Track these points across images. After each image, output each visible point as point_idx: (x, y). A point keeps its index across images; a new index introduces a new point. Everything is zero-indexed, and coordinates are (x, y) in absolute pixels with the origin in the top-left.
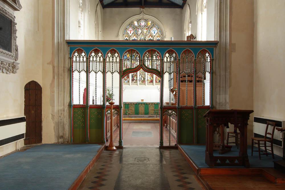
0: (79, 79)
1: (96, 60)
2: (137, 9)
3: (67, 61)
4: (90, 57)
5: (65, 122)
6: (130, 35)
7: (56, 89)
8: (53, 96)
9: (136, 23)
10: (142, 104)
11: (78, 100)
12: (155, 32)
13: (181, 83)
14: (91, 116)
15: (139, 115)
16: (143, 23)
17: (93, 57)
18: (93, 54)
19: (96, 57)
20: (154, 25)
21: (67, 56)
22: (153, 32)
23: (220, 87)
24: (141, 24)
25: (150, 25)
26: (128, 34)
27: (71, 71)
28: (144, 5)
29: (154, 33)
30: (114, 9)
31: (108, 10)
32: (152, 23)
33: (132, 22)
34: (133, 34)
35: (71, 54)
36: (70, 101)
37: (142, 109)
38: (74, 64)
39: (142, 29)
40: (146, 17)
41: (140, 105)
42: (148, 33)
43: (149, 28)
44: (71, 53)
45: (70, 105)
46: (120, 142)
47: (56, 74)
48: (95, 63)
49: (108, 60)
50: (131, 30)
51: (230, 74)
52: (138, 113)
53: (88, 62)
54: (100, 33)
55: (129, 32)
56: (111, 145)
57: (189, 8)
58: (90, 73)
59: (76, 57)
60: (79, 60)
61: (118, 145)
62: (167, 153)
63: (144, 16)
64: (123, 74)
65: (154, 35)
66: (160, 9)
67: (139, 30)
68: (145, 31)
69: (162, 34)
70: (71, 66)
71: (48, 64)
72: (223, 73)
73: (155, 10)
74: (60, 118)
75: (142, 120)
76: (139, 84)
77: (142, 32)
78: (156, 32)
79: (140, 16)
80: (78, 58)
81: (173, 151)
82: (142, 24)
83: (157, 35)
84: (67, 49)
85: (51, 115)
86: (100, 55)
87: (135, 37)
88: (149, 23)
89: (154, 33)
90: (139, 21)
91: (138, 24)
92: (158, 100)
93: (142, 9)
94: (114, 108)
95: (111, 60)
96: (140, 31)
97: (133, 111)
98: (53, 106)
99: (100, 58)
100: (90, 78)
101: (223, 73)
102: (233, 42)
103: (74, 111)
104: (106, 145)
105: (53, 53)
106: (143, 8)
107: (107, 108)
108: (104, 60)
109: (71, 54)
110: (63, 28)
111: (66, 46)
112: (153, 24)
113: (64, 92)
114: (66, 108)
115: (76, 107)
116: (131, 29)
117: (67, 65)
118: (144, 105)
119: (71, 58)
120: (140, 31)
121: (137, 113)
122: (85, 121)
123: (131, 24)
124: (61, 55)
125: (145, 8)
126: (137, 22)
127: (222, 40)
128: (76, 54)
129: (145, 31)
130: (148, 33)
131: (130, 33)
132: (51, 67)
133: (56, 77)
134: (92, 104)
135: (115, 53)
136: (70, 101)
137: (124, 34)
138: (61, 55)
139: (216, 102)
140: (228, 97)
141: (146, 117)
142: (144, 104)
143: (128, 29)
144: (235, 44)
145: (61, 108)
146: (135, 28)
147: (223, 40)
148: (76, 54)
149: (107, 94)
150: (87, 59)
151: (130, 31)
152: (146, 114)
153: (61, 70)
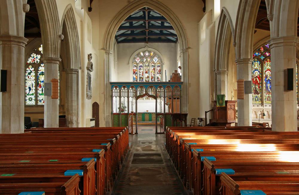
0: (116, 100)
1: (124, 90)
2: (143, 44)
3: (110, 92)
5: (110, 122)
6: (138, 62)
7: (105, 105)
8: (104, 109)
10: (147, 113)
11: (116, 110)
12: (156, 60)
13: (173, 100)
14: (122, 118)
15: (145, 121)
16: (147, 54)
18: (123, 88)
20: (155, 54)
21: (110, 89)
22: (155, 60)
23: (184, 103)
24: (145, 54)
25: (152, 55)
26: (136, 61)
27: (112, 97)
28: (148, 41)
31: (121, 44)
33: (139, 53)
35: (112, 88)
37: (147, 117)
38: (113, 93)
40: (150, 49)
41: (146, 114)
42: (151, 61)
43: (152, 58)
44: (112, 88)
45: (112, 113)
46: (136, 131)
47: (106, 99)
51: (188, 97)
52: (145, 120)
54: (116, 63)
55: (137, 61)
56: (132, 132)
59: (114, 90)
60: (115, 91)
62: (159, 135)
63: (148, 49)
64: (137, 98)
65: (156, 62)
66: (160, 44)
67: (145, 59)
68: (149, 60)
69: (161, 62)
72: (185, 97)
75: (147, 124)
77: (146, 60)
78: (157, 60)
79: (145, 49)
82: (146, 54)
84: (110, 86)
85: (103, 118)
86: (126, 88)
87: (141, 64)
89: (156, 61)
90: (144, 52)
91: (143, 54)
92: (155, 111)
93: (146, 44)
97: (141, 119)
98: (104, 114)
100: (121, 100)
101: (185, 97)
102: (190, 82)
106: (147, 43)
107: (130, 114)
108: (128, 92)
109: (112, 88)
110: (109, 76)
111: (110, 85)
112: (154, 54)
113: (109, 107)
114: (110, 115)
115: (114, 114)
116: (138, 58)
117: (110, 94)
118: (148, 114)
119: (112, 91)
120: (145, 60)
122: (119, 120)
123: (138, 54)
124: (108, 89)
125: (149, 43)
126: (143, 53)
129: (149, 60)
130: (151, 61)
131: (138, 61)
134: (226, 100)
135: (133, 88)
138: (108, 89)
139: (183, 111)
141: (150, 123)
142: (149, 113)
144: (190, 84)
145: (108, 114)
146: (142, 58)
147: (185, 81)
148: (114, 88)
149: (121, 107)
150: (120, 91)
152: (149, 121)
153: (108, 96)
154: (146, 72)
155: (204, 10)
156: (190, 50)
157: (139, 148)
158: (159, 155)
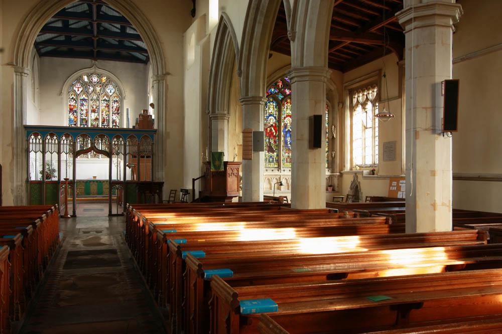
0: (35, 159)
1: (52, 142)
2: (87, 61)
3: (25, 143)
4: (46, 139)
9: (86, 78)
10: (93, 181)
11: (35, 174)
12: (111, 91)
16: (95, 79)
17: (49, 140)
19: (52, 140)
20: (109, 81)
21: (25, 138)
23: (158, 166)
25: (104, 81)
26: (75, 91)
27: (28, 152)
29: (111, 92)
30: (55, 59)
31: (47, 59)
32: (107, 78)
34: (82, 91)
35: (27, 138)
36: (28, 178)
37: (94, 188)
38: (31, 146)
39: (94, 86)
40: (100, 71)
42: (102, 92)
43: (104, 86)
46: (74, 212)
48: (50, 145)
49: (62, 142)
50: (78, 86)
53: (44, 144)
54: (37, 90)
55: (76, 89)
56: (66, 213)
57: (430, 237)
58: (46, 153)
60: (34, 142)
61: (72, 214)
62: (115, 219)
64: (76, 155)
65: (111, 94)
67: (91, 87)
68: (98, 89)
69: (121, 94)
70: (28, 148)
71: (8, 145)
73: (111, 64)
74: (18, 193)
76: (90, 156)
77: (93, 90)
78: (112, 91)
79: (92, 70)
80: (34, 141)
81: (119, 218)
83: (115, 95)
84: (24, 132)
85: (10, 190)
86: (55, 138)
87: (84, 95)
88: (104, 79)
91: (88, 79)
92: (108, 178)
93: (93, 62)
94: (68, 183)
95: (65, 142)
96: (91, 89)
98: (13, 182)
99: (55, 140)
101: (160, 155)
102: (168, 131)
103: (31, 188)
104: (62, 215)
105: (12, 137)
106: (95, 60)
111: (24, 130)
114: (24, 184)
115: (33, 182)
116: (78, 85)
117: (25, 147)
119: (28, 141)
120: (91, 89)
121: (88, 193)
123: (79, 79)
125: (98, 60)
126: (87, 76)
127: (160, 129)
128: (33, 137)
129: (98, 89)
130: (102, 92)
131: (78, 90)
132: (10, 148)
133: (15, 157)
136: (28, 178)
137: (69, 92)
140: (164, 173)
141: (99, 197)
142: (97, 181)
143: (75, 85)
145: (19, 183)
146: (85, 85)
150: (43, 141)
151: (78, 88)
153: (19, 150)
154: (94, 111)
155: (193, 13)
156: (169, 77)
157: (78, 242)
158: (113, 252)
